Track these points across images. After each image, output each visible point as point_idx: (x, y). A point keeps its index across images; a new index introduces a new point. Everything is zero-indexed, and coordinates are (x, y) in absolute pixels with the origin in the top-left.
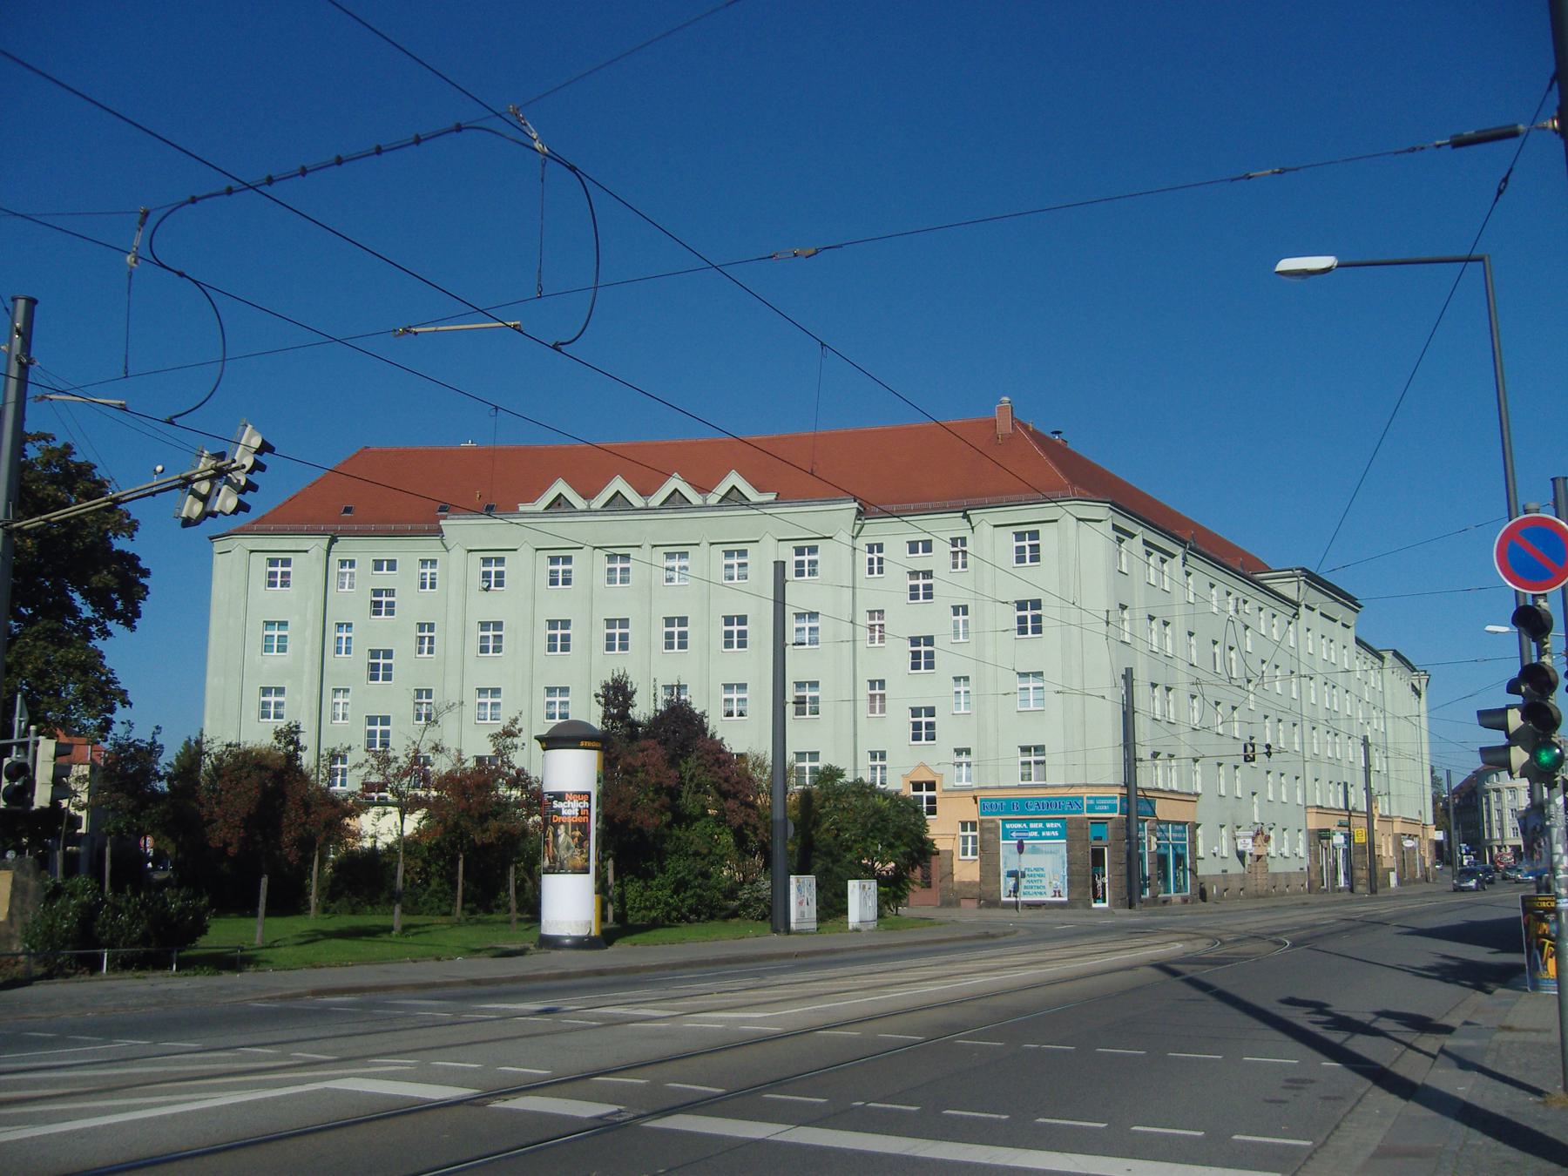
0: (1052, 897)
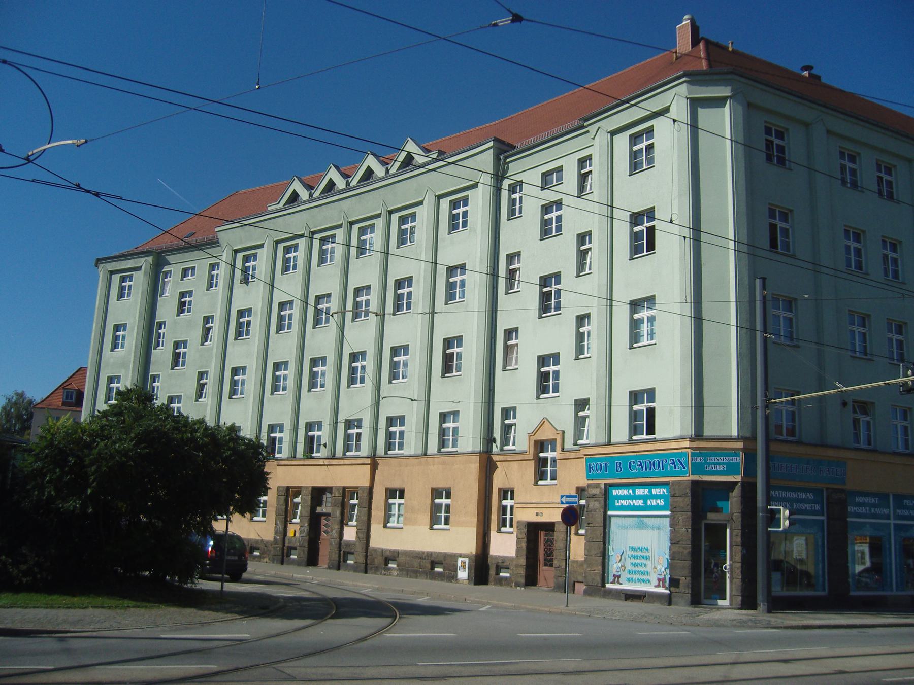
0: (655, 586)
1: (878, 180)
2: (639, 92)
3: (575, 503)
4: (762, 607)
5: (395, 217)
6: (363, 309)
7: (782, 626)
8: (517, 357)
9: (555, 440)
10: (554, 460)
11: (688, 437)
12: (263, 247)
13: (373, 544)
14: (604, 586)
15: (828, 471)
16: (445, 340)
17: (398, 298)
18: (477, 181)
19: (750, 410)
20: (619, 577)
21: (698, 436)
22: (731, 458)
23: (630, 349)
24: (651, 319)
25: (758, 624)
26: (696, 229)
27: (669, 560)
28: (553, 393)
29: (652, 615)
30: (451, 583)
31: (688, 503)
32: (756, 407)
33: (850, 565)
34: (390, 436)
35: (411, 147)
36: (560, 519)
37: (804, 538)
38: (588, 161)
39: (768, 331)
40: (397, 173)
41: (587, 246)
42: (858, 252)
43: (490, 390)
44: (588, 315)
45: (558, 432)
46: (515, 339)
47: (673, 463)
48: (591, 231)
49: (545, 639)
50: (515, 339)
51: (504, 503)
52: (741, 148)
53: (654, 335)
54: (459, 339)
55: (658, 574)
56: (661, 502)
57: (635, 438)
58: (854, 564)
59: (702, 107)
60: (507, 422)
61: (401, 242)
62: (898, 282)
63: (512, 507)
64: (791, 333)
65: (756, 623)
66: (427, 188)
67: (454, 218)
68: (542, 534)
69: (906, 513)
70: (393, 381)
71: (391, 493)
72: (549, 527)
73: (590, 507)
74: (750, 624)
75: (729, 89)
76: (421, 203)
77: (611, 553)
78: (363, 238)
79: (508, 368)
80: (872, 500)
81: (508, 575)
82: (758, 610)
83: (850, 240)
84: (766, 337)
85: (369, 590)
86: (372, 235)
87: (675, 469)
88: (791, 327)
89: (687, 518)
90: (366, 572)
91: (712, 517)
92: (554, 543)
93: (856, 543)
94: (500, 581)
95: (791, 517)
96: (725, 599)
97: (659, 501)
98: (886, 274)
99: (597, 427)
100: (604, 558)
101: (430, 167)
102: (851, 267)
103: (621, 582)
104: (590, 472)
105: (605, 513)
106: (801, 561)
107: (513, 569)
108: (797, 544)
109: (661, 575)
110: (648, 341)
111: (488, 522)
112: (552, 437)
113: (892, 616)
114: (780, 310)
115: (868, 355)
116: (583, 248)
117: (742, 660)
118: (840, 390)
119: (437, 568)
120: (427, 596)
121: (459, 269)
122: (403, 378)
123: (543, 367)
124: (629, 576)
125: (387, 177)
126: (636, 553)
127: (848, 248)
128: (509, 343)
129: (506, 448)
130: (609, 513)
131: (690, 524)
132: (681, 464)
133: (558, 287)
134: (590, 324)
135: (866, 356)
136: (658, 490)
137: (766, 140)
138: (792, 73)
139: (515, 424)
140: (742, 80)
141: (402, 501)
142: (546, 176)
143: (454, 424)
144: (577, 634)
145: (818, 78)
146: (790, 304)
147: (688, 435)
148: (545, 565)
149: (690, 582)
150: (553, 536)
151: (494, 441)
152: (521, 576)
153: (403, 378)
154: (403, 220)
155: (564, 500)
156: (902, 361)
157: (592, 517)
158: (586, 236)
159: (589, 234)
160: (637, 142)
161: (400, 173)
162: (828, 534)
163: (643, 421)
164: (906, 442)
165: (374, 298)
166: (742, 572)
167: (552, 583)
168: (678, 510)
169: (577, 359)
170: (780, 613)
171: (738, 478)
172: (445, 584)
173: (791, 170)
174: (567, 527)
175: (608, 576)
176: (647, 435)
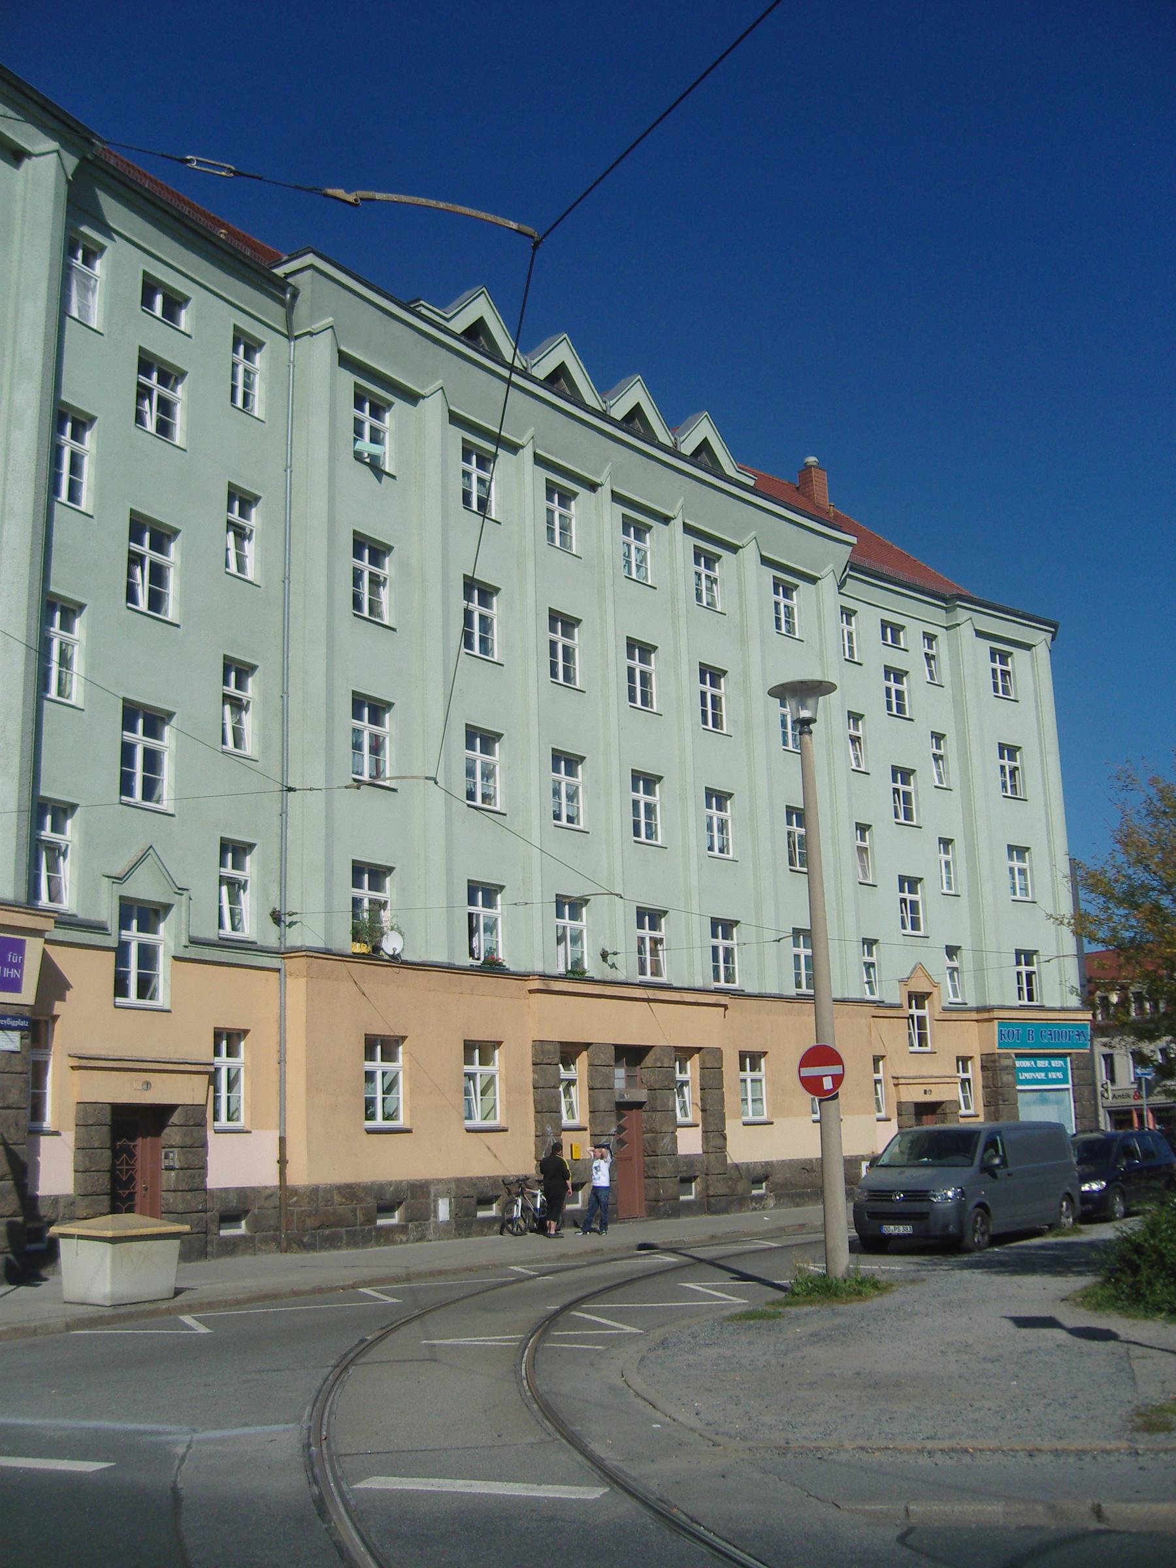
12: (463, 460)
97: (1058, 1074)
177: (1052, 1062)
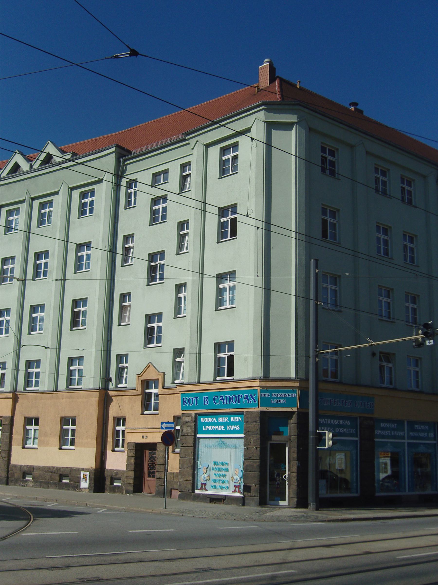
0: (233, 492)
1: (402, 190)
2: (229, 116)
3: (172, 428)
4: (312, 506)
5: (36, 203)
6: (9, 275)
7: (326, 520)
8: (129, 315)
9: (158, 379)
10: (157, 395)
11: (258, 378)
13: (14, 461)
14: (194, 492)
15: (361, 404)
16: (73, 301)
17: (37, 267)
18: (101, 178)
19: (304, 358)
20: (205, 485)
21: (266, 377)
22: (290, 394)
23: (216, 311)
24: (232, 289)
25: (309, 519)
26: (268, 222)
27: (243, 472)
28: (156, 343)
29: (230, 513)
30: (75, 492)
31: (258, 428)
32: (309, 356)
33: (376, 473)
34: (28, 375)
35: (51, 149)
36: (160, 441)
37: (343, 454)
38: (188, 166)
39: (319, 300)
40: (39, 169)
41: (185, 231)
42: (386, 242)
43: (108, 341)
44: (185, 284)
45: (160, 374)
46: (128, 302)
47: (247, 398)
48: (188, 220)
49: (148, 534)
50: (128, 302)
51: (118, 428)
52: (303, 162)
53: (234, 301)
54: (85, 301)
55: (235, 483)
56: (237, 428)
57: (218, 378)
58: (379, 472)
59: (275, 130)
60: (121, 365)
61: (41, 223)
62: (414, 265)
63: (124, 431)
64: (336, 301)
65: (308, 518)
66: (62, 182)
67: (83, 206)
68: (147, 453)
69: (416, 434)
70: (32, 333)
71: (28, 421)
72: (152, 447)
73: (183, 431)
74: (303, 518)
75: (296, 116)
76: (57, 193)
77: (199, 466)
78: (10, 219)
79: (122, 324)
80: (392, 425)
81: (120, 484)
82: (309, 509)
83: (380, 234)
84: (317, 304)
85: (10, 498)
86: (18, 217)
87: (248, 402)
88: (336, 297)
89: (257, 439)
90: (7, 484)
91: (275, 439)
92: (156, 459)
93: (381, 457)
94: (114, 490)
95: (334, 438)
96: (285, 500)
97: (236, 427)
98: (405, 260)
99: (190, 370)
100: (194, 470)
101: (64, 165)
102: (380, 253)
103: (206, 489)
104: (184, 405)
105: (195, 436)
106: (341, 471)
107: (124, 480)
108: (338, 458)
109: (237, 483)
110: (229, 305)
111: (105, 442)
112: (155, 378)
113: (405, 510)
114: (328, 284)
115: (391, 319)
116: (182, 233)
117: (297, 546)
118: (370, 344)
119: (64, 480)
120: (56, 502)
121: (86, 247)
122: (39, 330)
123: (149, 323)
124: (213, 484)
125: (31, 171)
126: (218, 467)
127: (378, 239)
128: (124, 304)
129: (119, 386)
130: (198, 436)
131: (259, 444)
132: (253, 398)
133: (162, 262)
134: (186, 291)
135: (390, 319)
136: (235, 418)
137: (322, 156)
138: (343, 108)
139: (127, 367)
140: (306, 110)
141: (37, 427)
142: (155, 176)
143: (79, 367)
144: (172, 530)
145: (361, 112)
146: (335, 279)
147: (258, 377)
148: (149, 476)
149: (259, 488)
150: (155, 453)
151: (111, 380)
152: (130, 485)
153: (39, 330)
154: (42, 206)
155: (164, 426)
156: (415, 322)
157: (185, 439)
158: (185, 223)
159: (187, 222)
160: (226, 154)
161: (41, 168)
162: (361, 450)
163: (225, 366)
164: (417, 382)
165: (17, 266)
166: (298, 480)
167: (154, 490)
168: (250, 433)
169: (175, 317)
170: (325, 510)
171: (295, 409)
172: (71, 492)
173: (340, 180)
174: (166, 447)
175: (197, 484)
176: (227, 376)
177: (220, 419)
